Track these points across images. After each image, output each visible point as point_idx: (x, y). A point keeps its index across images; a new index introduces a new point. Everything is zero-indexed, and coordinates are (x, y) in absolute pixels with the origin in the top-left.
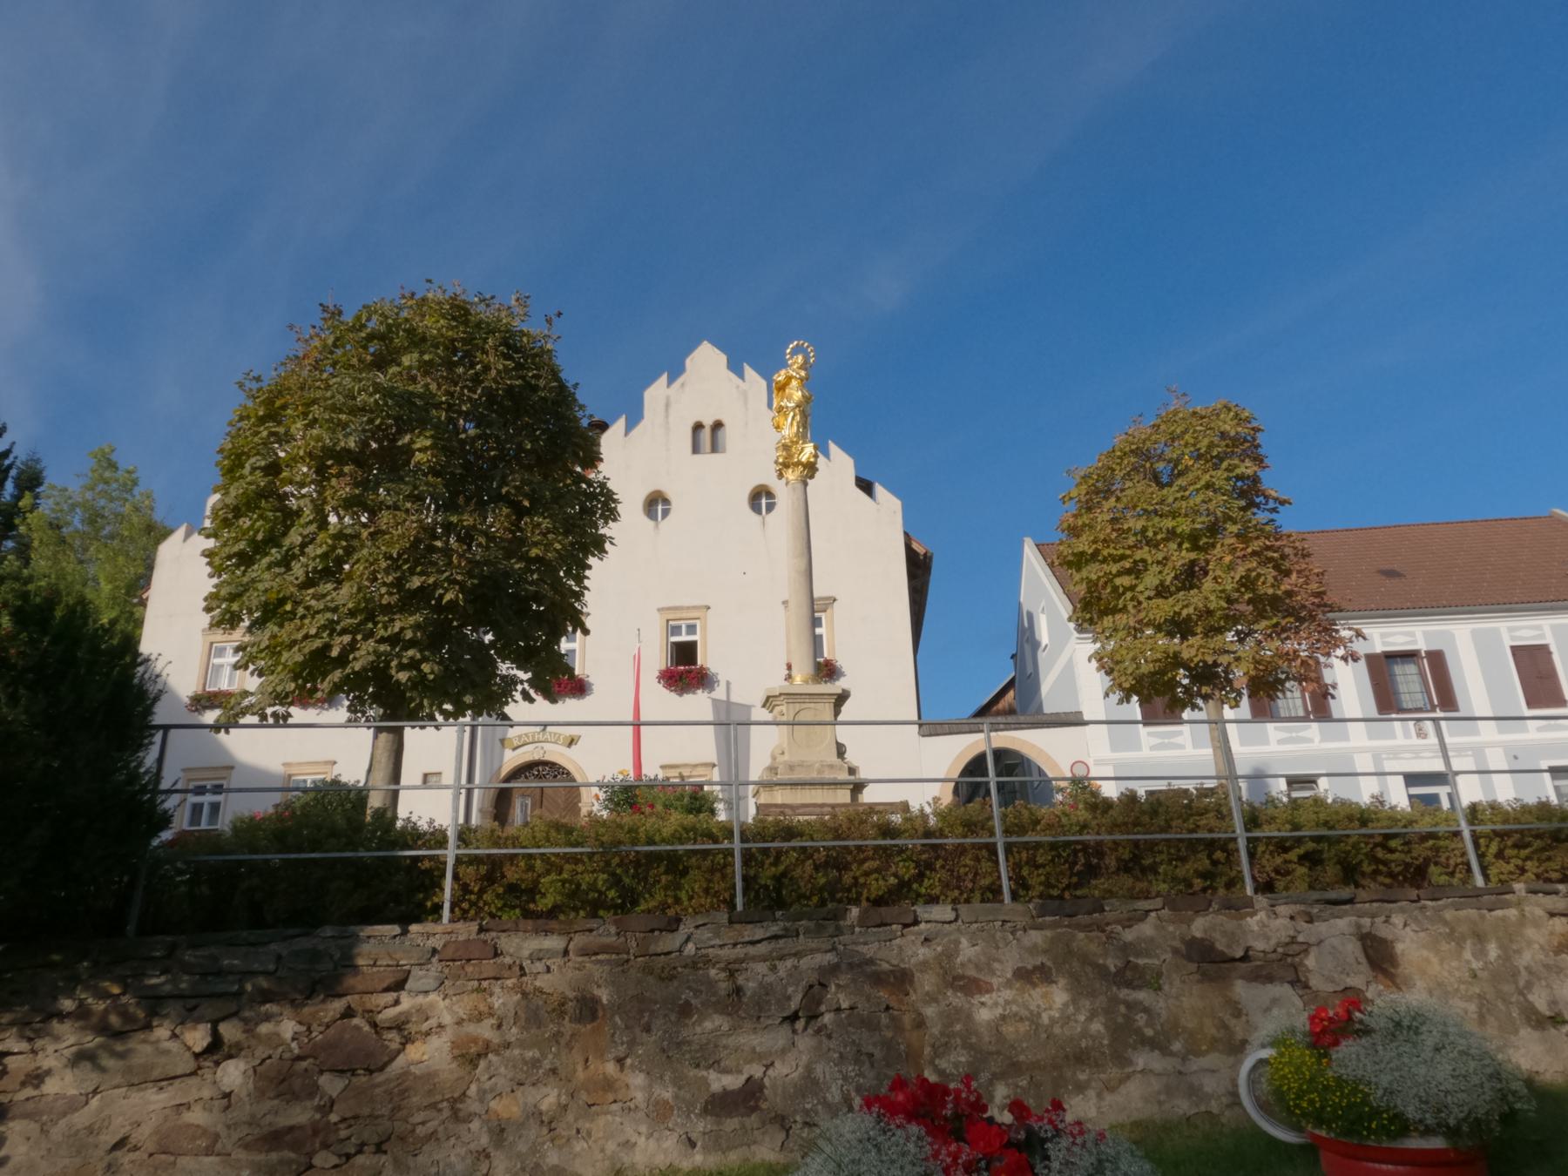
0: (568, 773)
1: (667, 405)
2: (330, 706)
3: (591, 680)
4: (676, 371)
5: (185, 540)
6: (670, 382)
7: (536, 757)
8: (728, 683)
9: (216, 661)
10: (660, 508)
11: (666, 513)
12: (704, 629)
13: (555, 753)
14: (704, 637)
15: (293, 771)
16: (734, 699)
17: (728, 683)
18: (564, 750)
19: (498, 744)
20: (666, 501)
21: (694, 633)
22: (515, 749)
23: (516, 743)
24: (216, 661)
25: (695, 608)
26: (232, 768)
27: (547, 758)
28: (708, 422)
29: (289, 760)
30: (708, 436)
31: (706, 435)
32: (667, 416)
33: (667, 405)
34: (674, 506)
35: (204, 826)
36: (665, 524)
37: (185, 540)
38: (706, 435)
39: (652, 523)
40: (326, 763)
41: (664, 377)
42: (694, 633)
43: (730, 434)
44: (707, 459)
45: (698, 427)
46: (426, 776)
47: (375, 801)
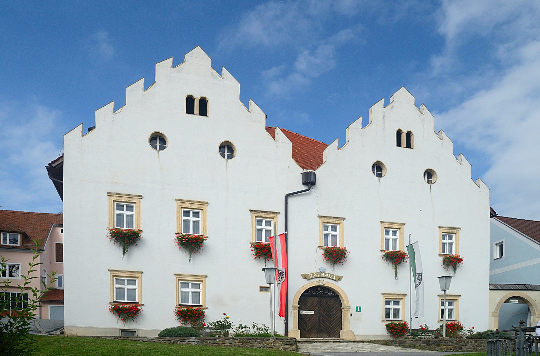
21: (336, 231)
30: (197, 106)
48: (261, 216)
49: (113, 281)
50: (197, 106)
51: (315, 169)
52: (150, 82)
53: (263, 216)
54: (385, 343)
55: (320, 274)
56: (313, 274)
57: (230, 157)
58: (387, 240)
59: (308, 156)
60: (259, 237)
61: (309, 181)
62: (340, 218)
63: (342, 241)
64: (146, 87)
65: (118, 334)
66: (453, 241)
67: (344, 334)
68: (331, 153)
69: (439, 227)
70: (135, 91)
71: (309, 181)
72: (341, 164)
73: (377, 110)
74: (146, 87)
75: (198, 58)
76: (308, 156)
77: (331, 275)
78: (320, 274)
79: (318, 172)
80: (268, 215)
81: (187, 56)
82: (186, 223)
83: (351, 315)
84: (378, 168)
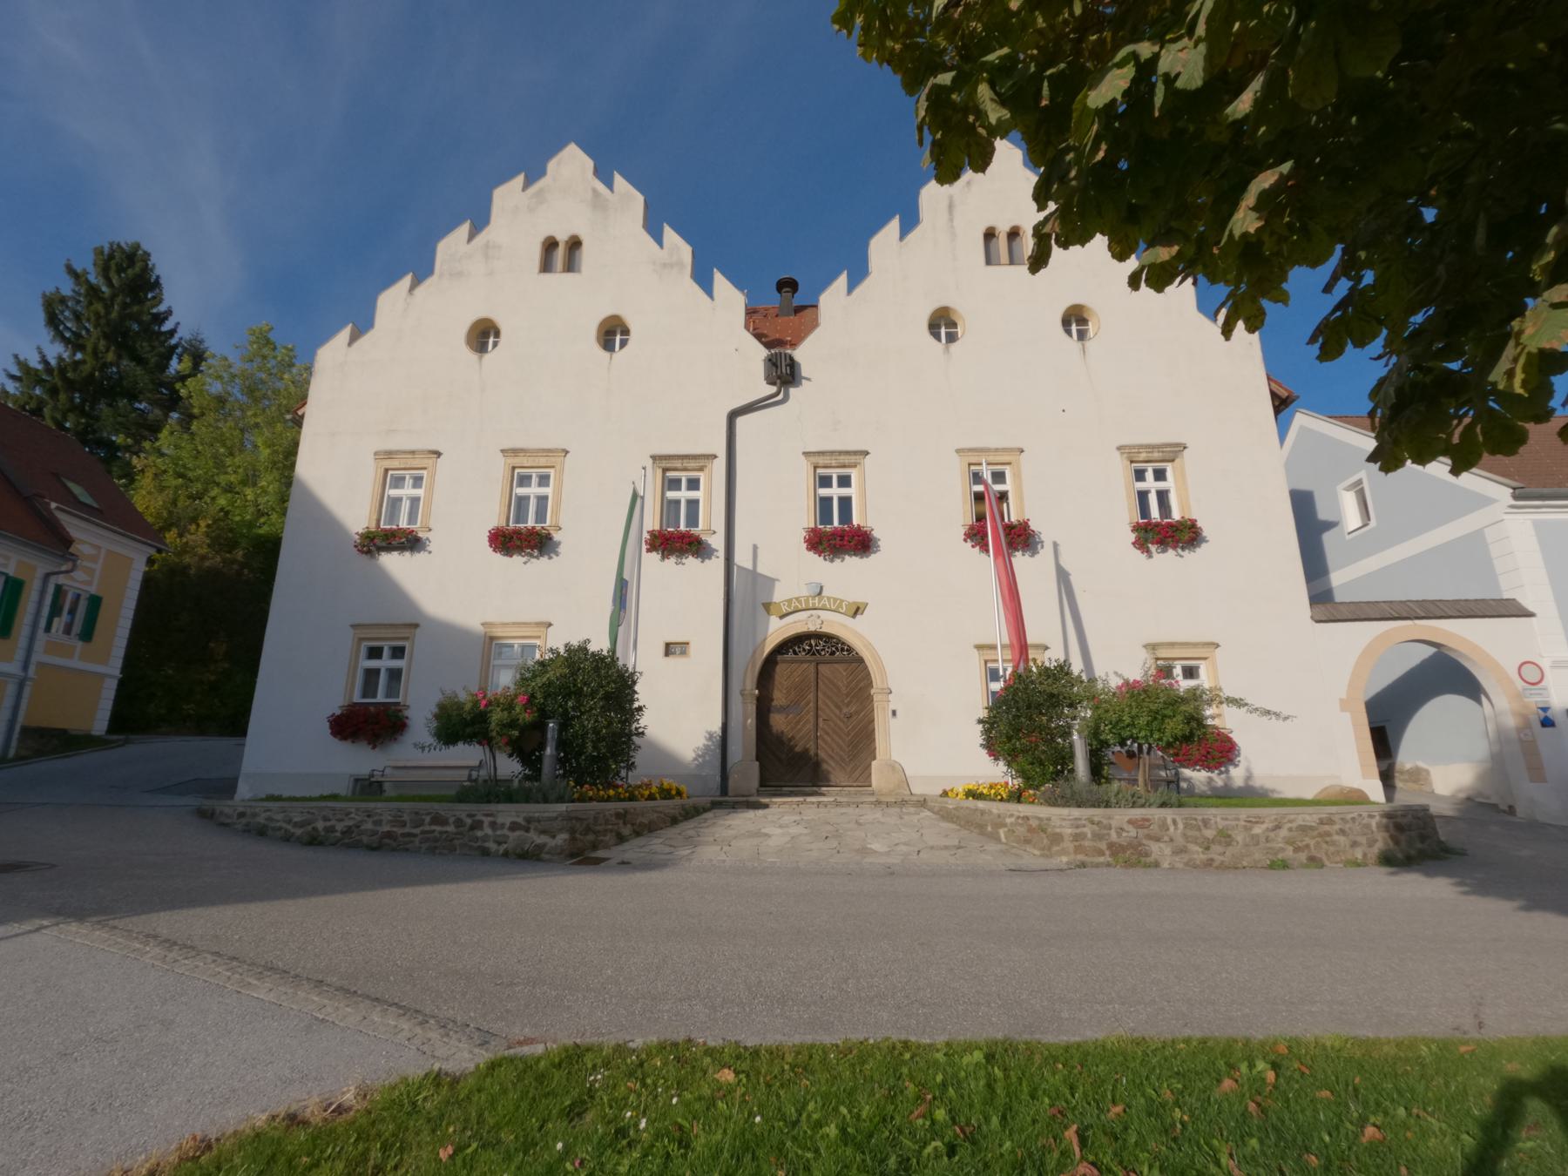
0: (850, 650)
1: (951, 207)
2: (541, 554)
3: (875, 534)
4: (534, 174)
5: (350, 344)
6: (527, 184)
7: (812, 629)
8: (1055, 545)
9: (394, 492)
10: (618, 338)
11: (623, 344)
12: (1017, 476)
13: (834, 623)
14: (558, 492)
15: (498, 632)
16: (760, 570)
17: (1055, 545)
18: (848, 621)
19: (761, 610)
20: (626, 332)
21: (697, 488)
22: (782, 617)
23: (785, 609)
24: (394, 492)
25: (1005, 450)
26: (416, 626)
27: (826, 629)
28: (562, 237)
29: (488, 620)
30: (561, 254)
31: (1002, 242)
32: (951, 220)
33: (951, 207)
34: (633, 338)
35: (380, 698)
36: (619, 355)
37: (350, 344)
38: (560, 254)
39: (606, 355)
40: (539, 624)
41: (520, 179)
42: (697, 488)
43: (587, 254)
44: (558, 279)
45: (990, 235)
46: (668, 645)
47: (1077, 667)
48: (674, 470)
49: (358, 650)
50: (561, 254)
51: (794, 345)
52: (910, 222)
53: (834, 463)
54: (1017, 796)
55: (807, 601)
56: (790, 601)
57: (952, 338)
58: (1143, 496)
59: (782, 317)
60: (521, 514)
61: (784, 374)
62: (855, 453)
63: (1021, 508)
64: (905, 231)
65: (343, 789)
66: (1169, 484)
67: (879, 777)
68: (833, 300)
69: (958, 451)
70: (884, 244)
71: (784, 374)
72: (853, 325)
73: (508, 197)
74: (905, 231)
75: (572, 165)
76: (782, 317)
77: (835, 600)
78: (807, 601)
79: (801, 354)
80: (692, 464)
81: (552, 166)
82: (1143, 496)
83: (894, 713)
84: (942, 324)
